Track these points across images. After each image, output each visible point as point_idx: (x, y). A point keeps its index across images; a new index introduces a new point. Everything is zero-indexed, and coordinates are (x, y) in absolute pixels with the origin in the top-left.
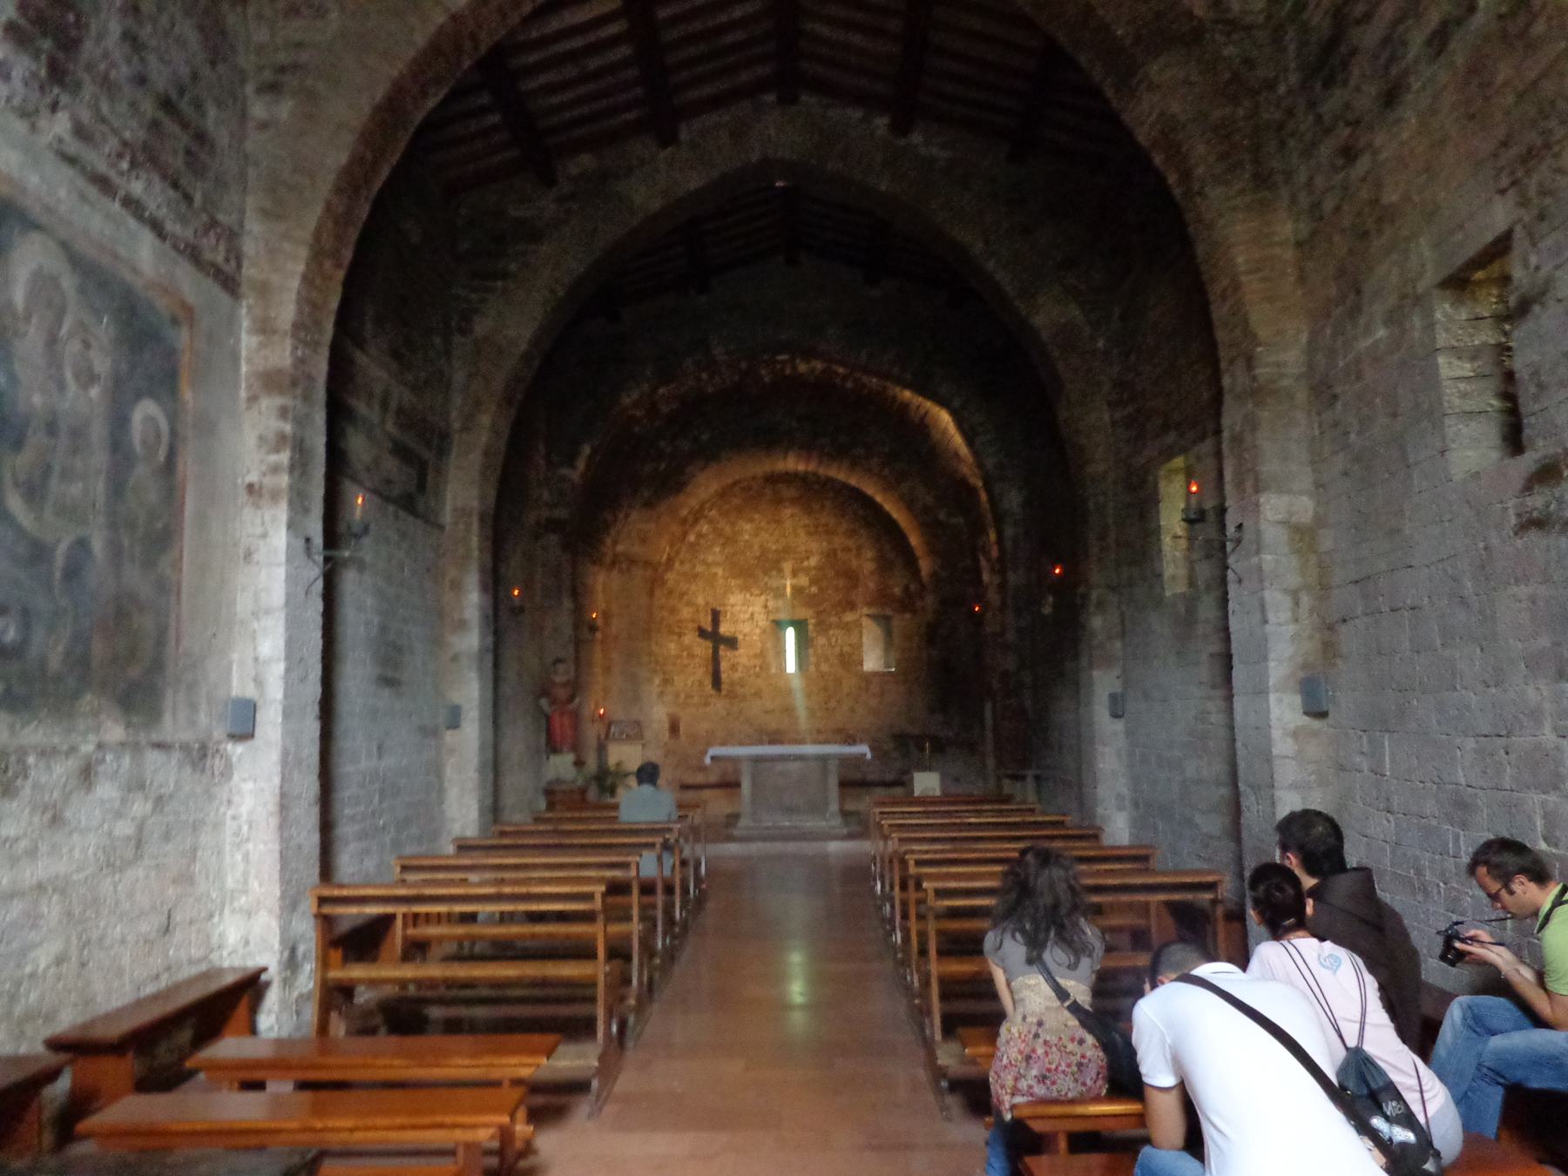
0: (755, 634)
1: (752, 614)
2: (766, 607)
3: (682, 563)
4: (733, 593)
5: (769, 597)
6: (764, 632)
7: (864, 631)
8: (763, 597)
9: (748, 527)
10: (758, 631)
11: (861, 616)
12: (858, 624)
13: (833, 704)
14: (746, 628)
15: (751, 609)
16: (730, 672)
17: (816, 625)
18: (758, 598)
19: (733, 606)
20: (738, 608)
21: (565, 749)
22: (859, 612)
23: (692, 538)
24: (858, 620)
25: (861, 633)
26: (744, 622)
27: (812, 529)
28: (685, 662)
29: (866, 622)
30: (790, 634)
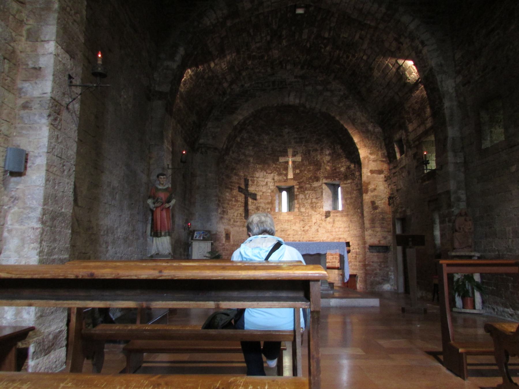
0: (268, 192)
1: (267, 183)
2: (274, 179)
3: (233, 152)
4: (258, 172)
6: (273, 191)
7: (324, 191)
8: (272, 174)
9: (266, 137)
10: (270, 191)
11: (322, 184)
12: (320, 187)
13: (307, 228)
15: (266, 180)
17: (298, 189)
18: (270, 175)
19: (257, 178)
20: (260, 179)
21: (163, 234)
23: (239, 139)
25: (322, 192)
26: (263, 186)
27: (298, 140)
28: (234, 203)
29: (324, 186)
30: (284, 194)
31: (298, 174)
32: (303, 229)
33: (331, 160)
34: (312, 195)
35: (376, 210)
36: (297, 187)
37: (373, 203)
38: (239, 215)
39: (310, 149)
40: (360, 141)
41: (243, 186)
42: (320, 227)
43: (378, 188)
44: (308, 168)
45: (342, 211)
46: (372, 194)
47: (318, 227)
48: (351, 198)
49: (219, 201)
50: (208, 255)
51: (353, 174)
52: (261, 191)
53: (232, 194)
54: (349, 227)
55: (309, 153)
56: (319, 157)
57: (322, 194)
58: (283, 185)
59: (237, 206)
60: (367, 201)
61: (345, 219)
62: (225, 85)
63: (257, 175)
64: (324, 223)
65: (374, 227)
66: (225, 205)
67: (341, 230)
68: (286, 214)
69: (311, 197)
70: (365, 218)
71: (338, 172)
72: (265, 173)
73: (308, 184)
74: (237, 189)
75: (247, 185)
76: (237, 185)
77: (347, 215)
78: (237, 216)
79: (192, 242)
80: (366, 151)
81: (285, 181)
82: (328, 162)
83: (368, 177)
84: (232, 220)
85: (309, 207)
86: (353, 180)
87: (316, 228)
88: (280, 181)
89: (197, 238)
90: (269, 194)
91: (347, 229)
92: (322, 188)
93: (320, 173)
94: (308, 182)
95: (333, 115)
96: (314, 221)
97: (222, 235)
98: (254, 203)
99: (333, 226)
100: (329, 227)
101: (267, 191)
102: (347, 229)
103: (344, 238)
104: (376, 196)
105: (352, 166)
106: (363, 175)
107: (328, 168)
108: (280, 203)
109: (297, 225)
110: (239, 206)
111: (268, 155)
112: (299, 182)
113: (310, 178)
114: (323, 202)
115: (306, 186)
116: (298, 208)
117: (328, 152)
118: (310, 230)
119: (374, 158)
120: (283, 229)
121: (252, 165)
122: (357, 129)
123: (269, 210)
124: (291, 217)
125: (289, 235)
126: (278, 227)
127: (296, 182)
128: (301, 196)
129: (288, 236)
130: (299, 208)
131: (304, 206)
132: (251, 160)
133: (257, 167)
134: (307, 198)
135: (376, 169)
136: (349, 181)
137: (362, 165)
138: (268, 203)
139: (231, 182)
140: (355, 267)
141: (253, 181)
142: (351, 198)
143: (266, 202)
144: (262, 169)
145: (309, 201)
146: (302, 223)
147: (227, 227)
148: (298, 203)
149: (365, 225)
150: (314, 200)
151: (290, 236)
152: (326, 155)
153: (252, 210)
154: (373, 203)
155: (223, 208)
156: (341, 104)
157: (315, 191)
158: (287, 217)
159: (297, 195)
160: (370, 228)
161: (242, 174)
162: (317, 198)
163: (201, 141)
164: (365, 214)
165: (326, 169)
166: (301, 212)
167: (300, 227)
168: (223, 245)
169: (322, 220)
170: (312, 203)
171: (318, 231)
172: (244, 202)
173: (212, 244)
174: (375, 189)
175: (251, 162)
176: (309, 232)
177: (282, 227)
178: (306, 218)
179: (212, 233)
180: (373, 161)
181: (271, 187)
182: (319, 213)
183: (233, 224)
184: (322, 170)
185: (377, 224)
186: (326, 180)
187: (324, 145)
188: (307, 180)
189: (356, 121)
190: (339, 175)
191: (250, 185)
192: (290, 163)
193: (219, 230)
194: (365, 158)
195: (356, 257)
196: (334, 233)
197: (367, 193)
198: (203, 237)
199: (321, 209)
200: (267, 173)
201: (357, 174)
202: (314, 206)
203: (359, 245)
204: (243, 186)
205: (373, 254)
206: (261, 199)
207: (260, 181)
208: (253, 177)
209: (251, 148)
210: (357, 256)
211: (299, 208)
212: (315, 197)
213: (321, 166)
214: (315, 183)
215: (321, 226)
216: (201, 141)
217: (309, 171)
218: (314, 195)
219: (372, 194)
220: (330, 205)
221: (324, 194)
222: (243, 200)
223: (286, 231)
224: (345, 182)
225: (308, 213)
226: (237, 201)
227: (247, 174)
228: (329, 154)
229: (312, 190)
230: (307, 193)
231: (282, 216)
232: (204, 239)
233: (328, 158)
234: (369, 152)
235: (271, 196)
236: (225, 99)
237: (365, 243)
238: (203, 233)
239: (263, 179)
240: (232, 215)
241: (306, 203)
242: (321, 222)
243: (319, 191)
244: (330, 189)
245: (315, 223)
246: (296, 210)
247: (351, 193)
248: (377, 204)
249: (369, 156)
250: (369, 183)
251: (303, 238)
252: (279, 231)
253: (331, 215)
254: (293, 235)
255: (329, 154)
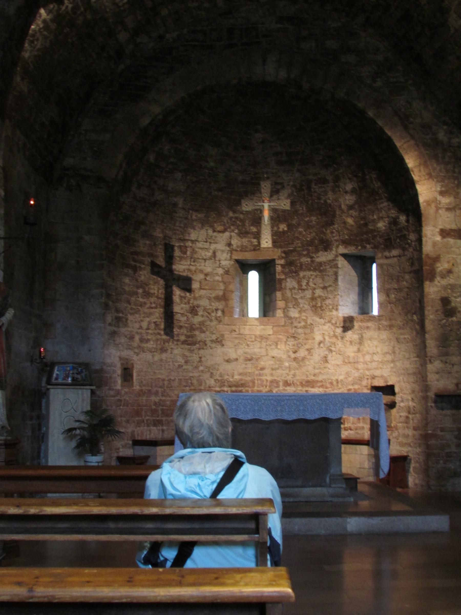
1: (214, 253)
2: (229, 245)
4: (194, 229)
5: (233, 234)
6: (227, 272)
7: (340, 273)
8: (227, 234)
10: (220, 271)
11: (336, 256)
12: (333, 264)
13: (302, 353)
14: (208, 267)
15: (213, 246)
16: (190, 315)
18: (221, 235)
19: (193, 241)
20: (199, 245)
22: (334, 252)
23: (152, 157)
24: (333, 260)
25: (336, 274)
26: (205, 260)
29: (341, 262)
31: (284, 232)
32: (293, 356)
33: (356, 203)
34: (315, 281)
35: (452, 316)
36: (282, 262)
37: (445, 301)
38: (153, 326)
39: (311, 177)
40: (420, 165)
41: (161, 261)
42: (331, 351)
43: (456, 270)
44: (307, 219)
45: (380, 317)
46: (444, 282)
47: (327, 353)
48: (399, 290)
49: (108, 296)
50: (83, 418)
51: (404, 237)
52: (201, 271)
53: (137, 280)
54: (394, 352)
55: (309, 188)
56: (330, 195)
57: (336, 279)
58: (249, 256)
59: (148, 305)
60: (433, 296)
61: (384, 335)
62: (123, 36)
63: (193, 235)
64: (340, 344)
65: (447, 354)
66: (122, 305)
67: (376, 358)
68: (256, 323)
69: (311, 284)
70: (427, 336)
71: (372, 231)
72: (210, 232)
73: (305, 256)
74: (149, 268)
75: (170, 259)
76: (148, 260)
77: (391, 327)
78: (148, 329)
79: (48, 389)
80: (431, 188)
81: (254, 250)
82: (351, 207)
83: (435, 244)
84: (137, 338)
85: (306, 307)
86: (404, 249)
87: (323, 354)
88: (243, 249)
89: (60, 381)
90: (217, 278)
91: (389, 357)
92: (336, 266)
93: (332, 233)
94: (305, 253)
95: (360, 105)
96: (318, 338)
97: (114, 372)
98: (185, 298)
99: (359, 350)
100: (351, 351)
101: (215, 272)
102: (389, 357)
103: (382, 376)
104: (453, 287)
105: (403, 218)
106: (424, 239)
107: (350, 221)
108: (244, 298)
109: (281, 346)
110: (153, 305)
111: (219, 190)
112: (285, 252)
113: (311, 243)
114: (339, 297)
115: (302, 260)
116: (284, 309)
117: (349, 187)
118: (308, 357)
119: (450, 203)
120: (249, 357)
121: (181, 213)
122: (412, 137)
123: (219, 313)
124: (269, 330)
125: (262, 369)
126: (240, 352)
127: (280, 250)
128: (290, 283)
129: (261, 372)
130: (285, 310)
131: (296, 304)
132: (180, 202)
133: (194, 217)
134: (304, 287)
135: (454, 227)
136: (395, 252)
137: (423, 219)
138: (217, 298)
139: (136, 253)
140: (405, 441)
141: (184, 250)
142: (399, 290)
143: (213, 295)
144: (204, 223)
145: (308, 294)
146: (291, 342)
147: (126, 353)
148: (285, 299)
149: (428, 350)
150: (318, 292)
151: (265, 371)
152: (346, 192)
153: (182, 314)
154: (445, 301)
155: (117, 311)
156: (379, 83)
157: (321, 271)
158: (258, 330)
159: (281, 280)
160: (440, 356)
161: (158, 234)
162: (325, 288)
163: (69, 161)
164: (429, 326)
165: (345, 223)
166: (290, 318)
167: (288, 351)
168: (118, 393)
169: (335, 336)
170: (313, 299)
171: (326, 361)
172: (163, 296)
173: (93, 392)
174: (450, 272)
175: (180, 206)
176: (307, 363)
177: (247, 350)
178: (300, 331)
179: (93, 368)
180: (448, 209)
181: (224, 263)
182: (329, 322)
183: (139, 347)
184: (336, 226)
185: (453, 349)
186: (346, 247)
187: (341, 171)
188: (303, 246)
189: (411, 120)
190: (374, 237)
191: (178, 259)
192: (266, 215)
193: (108, 361)
194: (428, 203)
195: (407, 417)
196: (361, 366)
197: (432, 280)
198: (73, 379)
199: (334, 313)
200: (214, 231)
201: (412, 237)
202: (319, 304)
203: (413, 392)
204: (161, 261)
205: (444, 412)
206: (201, 288)
207: (201, 248)
208: (184, 240)
209: (178, 175)
210: (410, 416)
211: (285, 310)
212: (322, 285)
213: (334, 216)
214: (321, 253)
215: (333, 349)
216: (69, 161)
217: (308, 227)
218: (319, 280)
219: (444, 282)
220: (353, 303)
221: (340, 278)
222: (162, 291)
223: (257, 359)
224: (387, 254)
225: (305, 321)
226: (147, 294)
227: (169, 233)
228: (353, 191)
229: (315, 270)
230: (304, 277)
231: (247, 327)
232: (76, 383)
233: (350, 199)
234: (439, 189)
235: (225, 283)
236: (122, 67)
237: (426, 388)
238: (73, 368)
239: (206, 245)
240: (137, 325)
241: (302, 298)
242: (334, 340)
243: (331, 272)
244: (354, 267)
245: (320, 343)
246: (279, 313)
247: (398, 279)
248: (453, 304)
249: (439, 198)
250: (437, 259)
251: (294, 375)
252: (241, 360)
253: (356, 325)
254: (273, 369)
255: (353, 191)
